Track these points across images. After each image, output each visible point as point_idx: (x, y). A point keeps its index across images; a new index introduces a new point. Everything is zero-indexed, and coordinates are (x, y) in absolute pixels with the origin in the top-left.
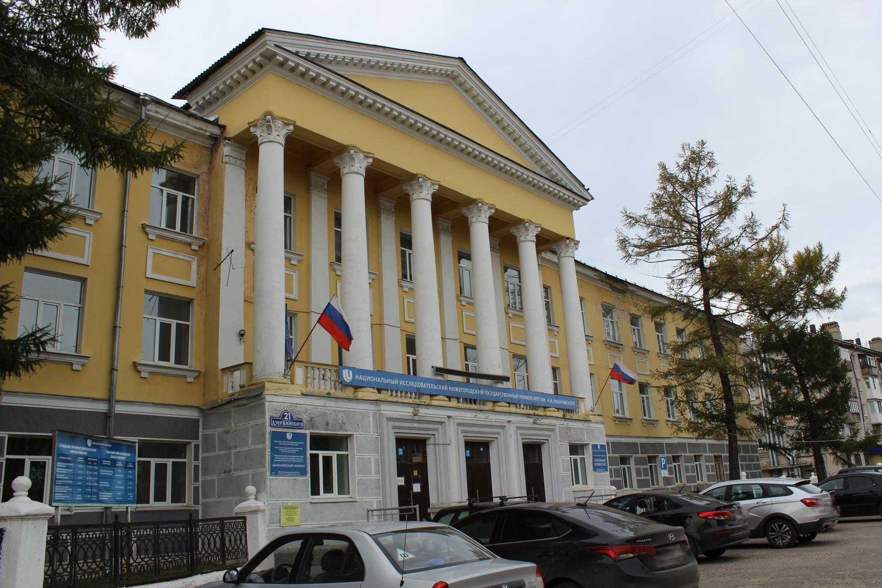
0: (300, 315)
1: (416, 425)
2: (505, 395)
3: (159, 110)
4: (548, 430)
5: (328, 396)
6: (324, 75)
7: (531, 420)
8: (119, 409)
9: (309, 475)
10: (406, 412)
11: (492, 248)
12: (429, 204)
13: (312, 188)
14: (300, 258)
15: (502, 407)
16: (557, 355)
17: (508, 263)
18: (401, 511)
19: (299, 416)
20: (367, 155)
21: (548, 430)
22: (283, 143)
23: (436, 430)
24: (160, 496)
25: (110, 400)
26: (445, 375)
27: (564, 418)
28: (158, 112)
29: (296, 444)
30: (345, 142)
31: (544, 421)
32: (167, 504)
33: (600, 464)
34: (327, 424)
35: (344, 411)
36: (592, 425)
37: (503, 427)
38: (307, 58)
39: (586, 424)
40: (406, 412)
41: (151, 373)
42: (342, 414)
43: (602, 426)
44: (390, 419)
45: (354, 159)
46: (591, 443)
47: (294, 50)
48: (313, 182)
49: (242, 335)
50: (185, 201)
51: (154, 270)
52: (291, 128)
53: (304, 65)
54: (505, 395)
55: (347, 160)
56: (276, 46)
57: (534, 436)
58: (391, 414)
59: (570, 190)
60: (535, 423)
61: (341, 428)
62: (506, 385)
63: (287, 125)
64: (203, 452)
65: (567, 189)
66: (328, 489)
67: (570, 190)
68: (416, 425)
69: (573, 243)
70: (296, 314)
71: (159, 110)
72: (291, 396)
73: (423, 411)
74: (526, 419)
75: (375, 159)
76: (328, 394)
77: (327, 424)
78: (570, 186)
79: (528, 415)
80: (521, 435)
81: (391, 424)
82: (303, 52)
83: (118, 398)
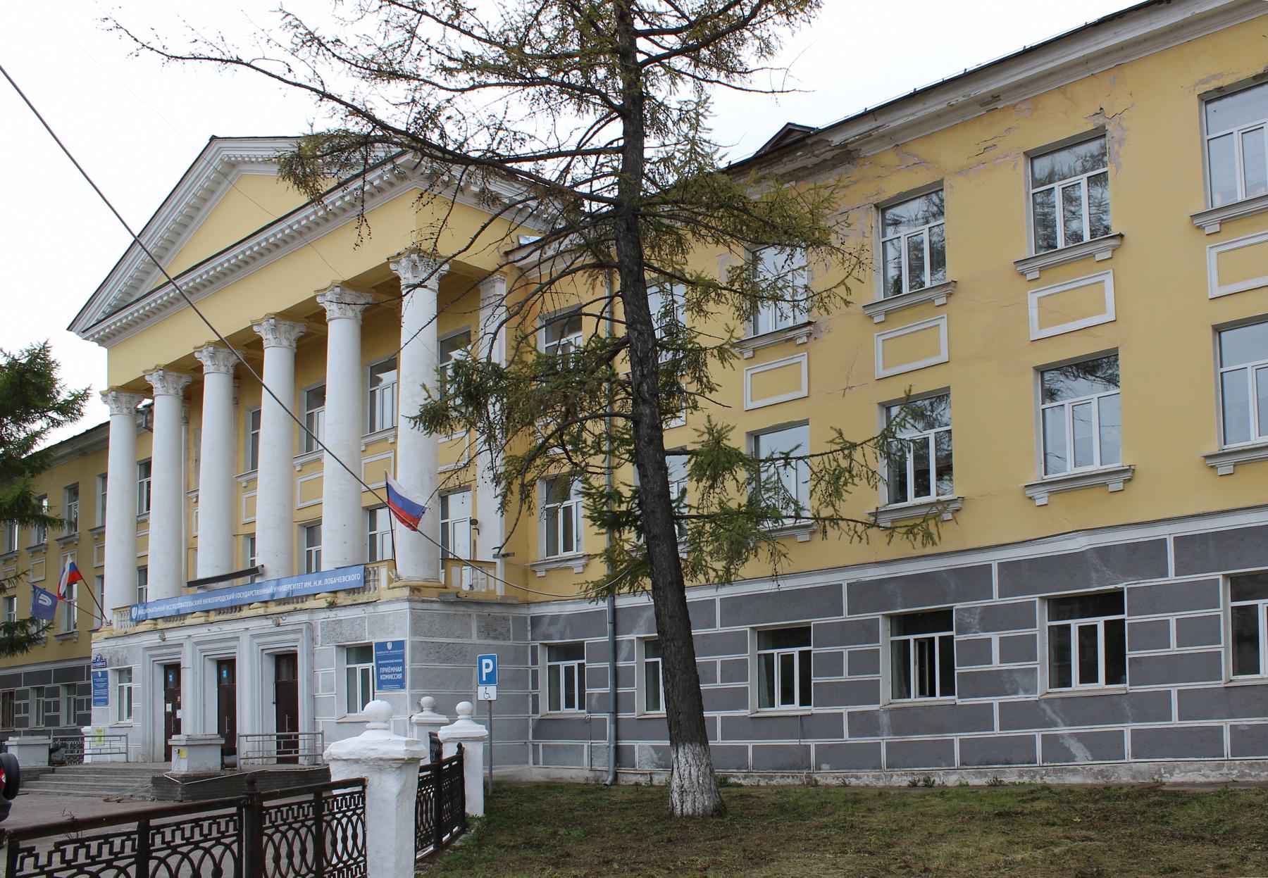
1: (164, 651)
4: (294, 631)
5: (126, 635)
7: (269, 622)
9: (1127, 657)
10: (154, 639)
12: (433, 296)
18: (278, 737)
21: (294, 631)
24: (570, 704)
32: (795, 709)
33: (390, 677)
36: (382, 609)
39: (370, 609)
51: (1103, 310)
57: (282, 643)
58: (147, 644)
66: (787, 698)
68: (164, 651)
79: (265, 616)
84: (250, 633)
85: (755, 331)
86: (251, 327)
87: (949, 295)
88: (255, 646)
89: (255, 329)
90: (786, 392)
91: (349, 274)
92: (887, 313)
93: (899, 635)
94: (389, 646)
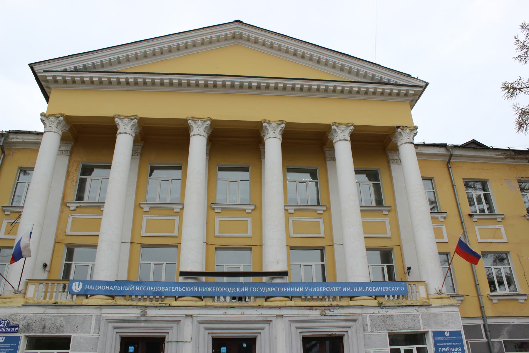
0: (326, 247)
1: (142, 325)
2: (282, 290)
3: (18, 137)
6: (105, 77)
7: (318, 312)
8: (490, 321)
11: (134, 152)
13: (391, 163)
14: (390, 209)
15: (276, 302)
16: (446, 240)
17: (90, 160)
19: (16, 323)
20: (131, 118)
22: (349, 139)
23: (171, 328)
25: (483, 317)
26: (200, 278)
27: (380, 305)
28: (18, 138)
29: (8, 345)
30: (111, 115)
31: (338, 311)
34: (44, 327)
35: (64, 316)
36: (432, 310)
37: (269, 322)
38: (76, 70)
39: (423, 309)
40: (134, 313)
41: (499, 300)
42: (62, 319)
43: (457, 309)
44: (110, 321)
45: (401, 134)
46: (431, 330)
47: (61, 69)
48: (327, 155)
49: (45, 266)
50: (485, 195)
51: (481, 238)
52: (352, 128)
53: (77, 76)
54: (282, 290)
55: (334, 134)
56: (44, 71)
58: (110, 316)
59: (396, 84)
60: (322, 315)
61: (58, 330)
62: (286, 279)
63: (280, 124)
64: (417, 348)
65: (386, 84)
67: (396, 84)
68: (142, 325)
69: (408, 131)
70: (324, 248)
71: (24, 137)
72: (13, 307)
73: (151, 312)
74: (307, 312)
75: (355, 126)
76: (55, 303)
77: (44, 327)
78: (393, 80)
80: (297, 328)
81: (111, 325)
82: (70, 67)
83: (487, 315)
84: (286, 320)
85: (12, 205)
86: (113, 118)
87: (389, 211)
88: (293, 329)
89: (116, 119)
90: (381, 234)
91: (68, 114)
92: (295, 210)
93: (424, 348)
94: (447, 334)
